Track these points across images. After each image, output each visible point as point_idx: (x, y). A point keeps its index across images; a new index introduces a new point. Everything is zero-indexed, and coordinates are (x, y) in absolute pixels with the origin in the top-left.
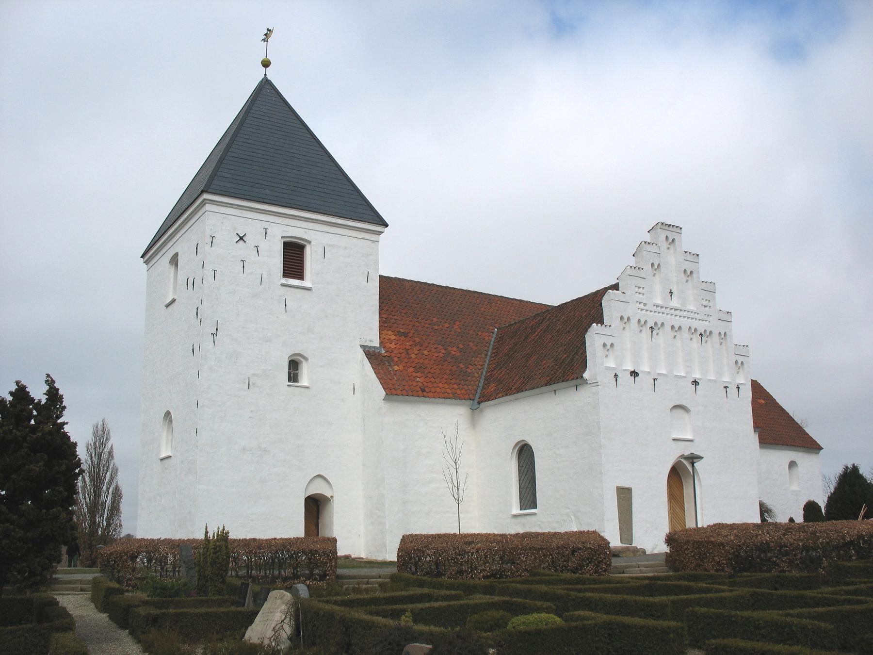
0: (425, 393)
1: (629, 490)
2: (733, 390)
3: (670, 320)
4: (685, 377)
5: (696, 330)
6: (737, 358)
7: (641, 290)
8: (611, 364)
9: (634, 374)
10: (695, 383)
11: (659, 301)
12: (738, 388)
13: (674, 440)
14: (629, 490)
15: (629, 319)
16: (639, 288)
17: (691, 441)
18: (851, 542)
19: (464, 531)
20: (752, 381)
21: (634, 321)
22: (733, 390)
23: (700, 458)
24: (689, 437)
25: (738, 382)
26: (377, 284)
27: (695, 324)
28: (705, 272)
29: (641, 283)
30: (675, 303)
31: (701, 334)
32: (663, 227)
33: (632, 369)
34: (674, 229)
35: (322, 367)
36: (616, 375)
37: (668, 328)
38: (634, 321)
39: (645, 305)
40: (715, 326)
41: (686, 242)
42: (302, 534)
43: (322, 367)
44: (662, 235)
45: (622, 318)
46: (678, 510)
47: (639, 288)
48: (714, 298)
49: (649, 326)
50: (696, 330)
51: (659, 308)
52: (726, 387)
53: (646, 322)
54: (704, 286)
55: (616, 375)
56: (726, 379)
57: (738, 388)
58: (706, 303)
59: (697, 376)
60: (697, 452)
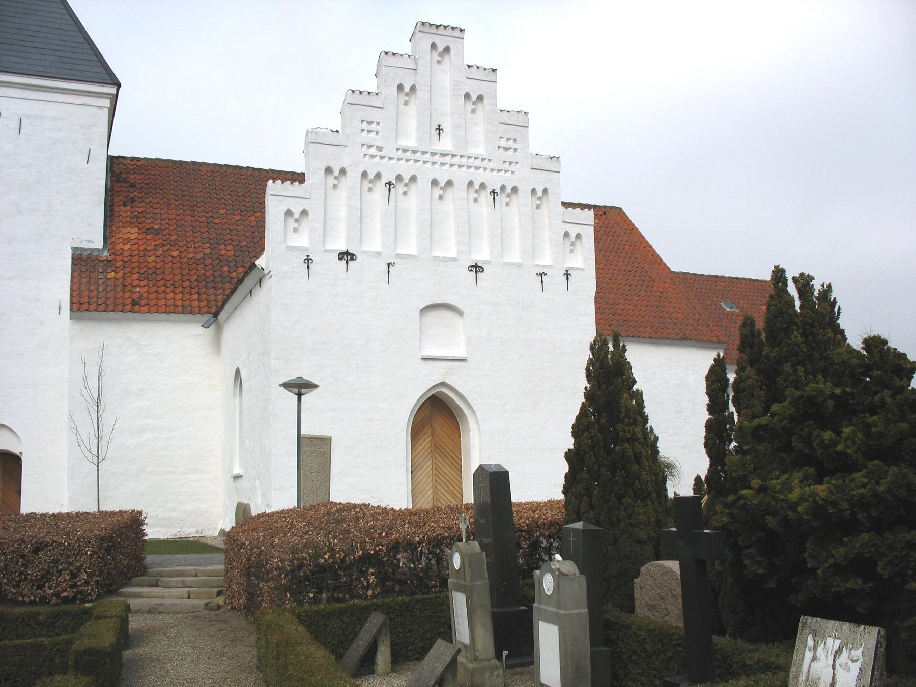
0: (137, 308)
1: (324, 443)
2: (556, 279)
3: (426, 173)
4: (455, 260)
5: (483, 186)
6: (568, 228)
7: (373, 127)
8: (302, 240)
9: (347, 256)
10: (477, 268)
11: (411, 143)
12: (567, 275)
13: (425, 359)
14: (324, 443)
15: (343, 171)
16: (370, 123)
17: (463, 360)
18: (368, 559)
19: (107, 507)
20: (829, 287)
21: (354, 175)
22: (556, 279)
23: (311, 386)
24: (460, 353)
25: (568, 265)
26: (103, 164)
27: (479, 177)
28: (507, 95)
29: (374, 115)
30: (446, 144)
31: (493, 192)
32: (427, 29)
33: (344, 249)
34: (449, 32)
35: (10, 279)
36: (308, 259)
37: (424, 183)
38: (354, 175)
39: (380, 149)
40: (524, 178)
41: (473, 51)
42: (25, 509)
43: (10, 279)
44: (425, 42)
45: (329, 170)
46: (447, 469)
47: (370, 123)
48: (525, 137)
49: (384, 180)
50: (483, 186)
51: (408, 154)
52: (541, 275)
53: (378, 176)
54: (505, 117)
55: (308, 259)
56: (546, 260)
57: (567, 275)
58: (510, 144)
59: (479, 257)
60: (308, 377)
